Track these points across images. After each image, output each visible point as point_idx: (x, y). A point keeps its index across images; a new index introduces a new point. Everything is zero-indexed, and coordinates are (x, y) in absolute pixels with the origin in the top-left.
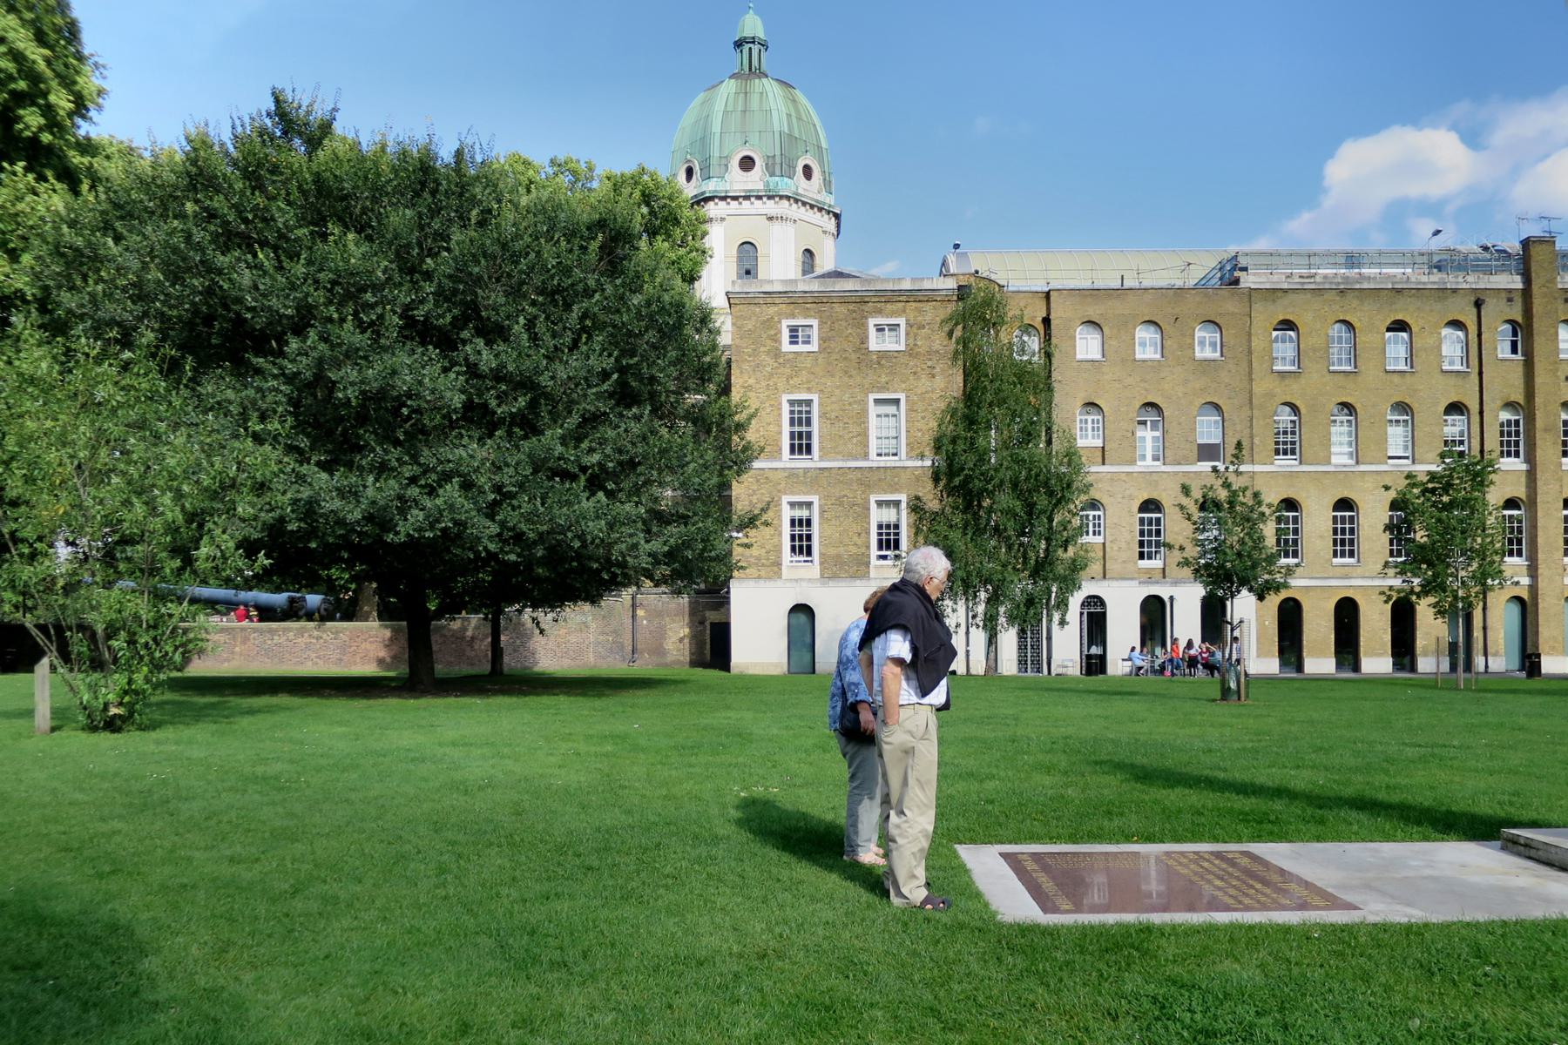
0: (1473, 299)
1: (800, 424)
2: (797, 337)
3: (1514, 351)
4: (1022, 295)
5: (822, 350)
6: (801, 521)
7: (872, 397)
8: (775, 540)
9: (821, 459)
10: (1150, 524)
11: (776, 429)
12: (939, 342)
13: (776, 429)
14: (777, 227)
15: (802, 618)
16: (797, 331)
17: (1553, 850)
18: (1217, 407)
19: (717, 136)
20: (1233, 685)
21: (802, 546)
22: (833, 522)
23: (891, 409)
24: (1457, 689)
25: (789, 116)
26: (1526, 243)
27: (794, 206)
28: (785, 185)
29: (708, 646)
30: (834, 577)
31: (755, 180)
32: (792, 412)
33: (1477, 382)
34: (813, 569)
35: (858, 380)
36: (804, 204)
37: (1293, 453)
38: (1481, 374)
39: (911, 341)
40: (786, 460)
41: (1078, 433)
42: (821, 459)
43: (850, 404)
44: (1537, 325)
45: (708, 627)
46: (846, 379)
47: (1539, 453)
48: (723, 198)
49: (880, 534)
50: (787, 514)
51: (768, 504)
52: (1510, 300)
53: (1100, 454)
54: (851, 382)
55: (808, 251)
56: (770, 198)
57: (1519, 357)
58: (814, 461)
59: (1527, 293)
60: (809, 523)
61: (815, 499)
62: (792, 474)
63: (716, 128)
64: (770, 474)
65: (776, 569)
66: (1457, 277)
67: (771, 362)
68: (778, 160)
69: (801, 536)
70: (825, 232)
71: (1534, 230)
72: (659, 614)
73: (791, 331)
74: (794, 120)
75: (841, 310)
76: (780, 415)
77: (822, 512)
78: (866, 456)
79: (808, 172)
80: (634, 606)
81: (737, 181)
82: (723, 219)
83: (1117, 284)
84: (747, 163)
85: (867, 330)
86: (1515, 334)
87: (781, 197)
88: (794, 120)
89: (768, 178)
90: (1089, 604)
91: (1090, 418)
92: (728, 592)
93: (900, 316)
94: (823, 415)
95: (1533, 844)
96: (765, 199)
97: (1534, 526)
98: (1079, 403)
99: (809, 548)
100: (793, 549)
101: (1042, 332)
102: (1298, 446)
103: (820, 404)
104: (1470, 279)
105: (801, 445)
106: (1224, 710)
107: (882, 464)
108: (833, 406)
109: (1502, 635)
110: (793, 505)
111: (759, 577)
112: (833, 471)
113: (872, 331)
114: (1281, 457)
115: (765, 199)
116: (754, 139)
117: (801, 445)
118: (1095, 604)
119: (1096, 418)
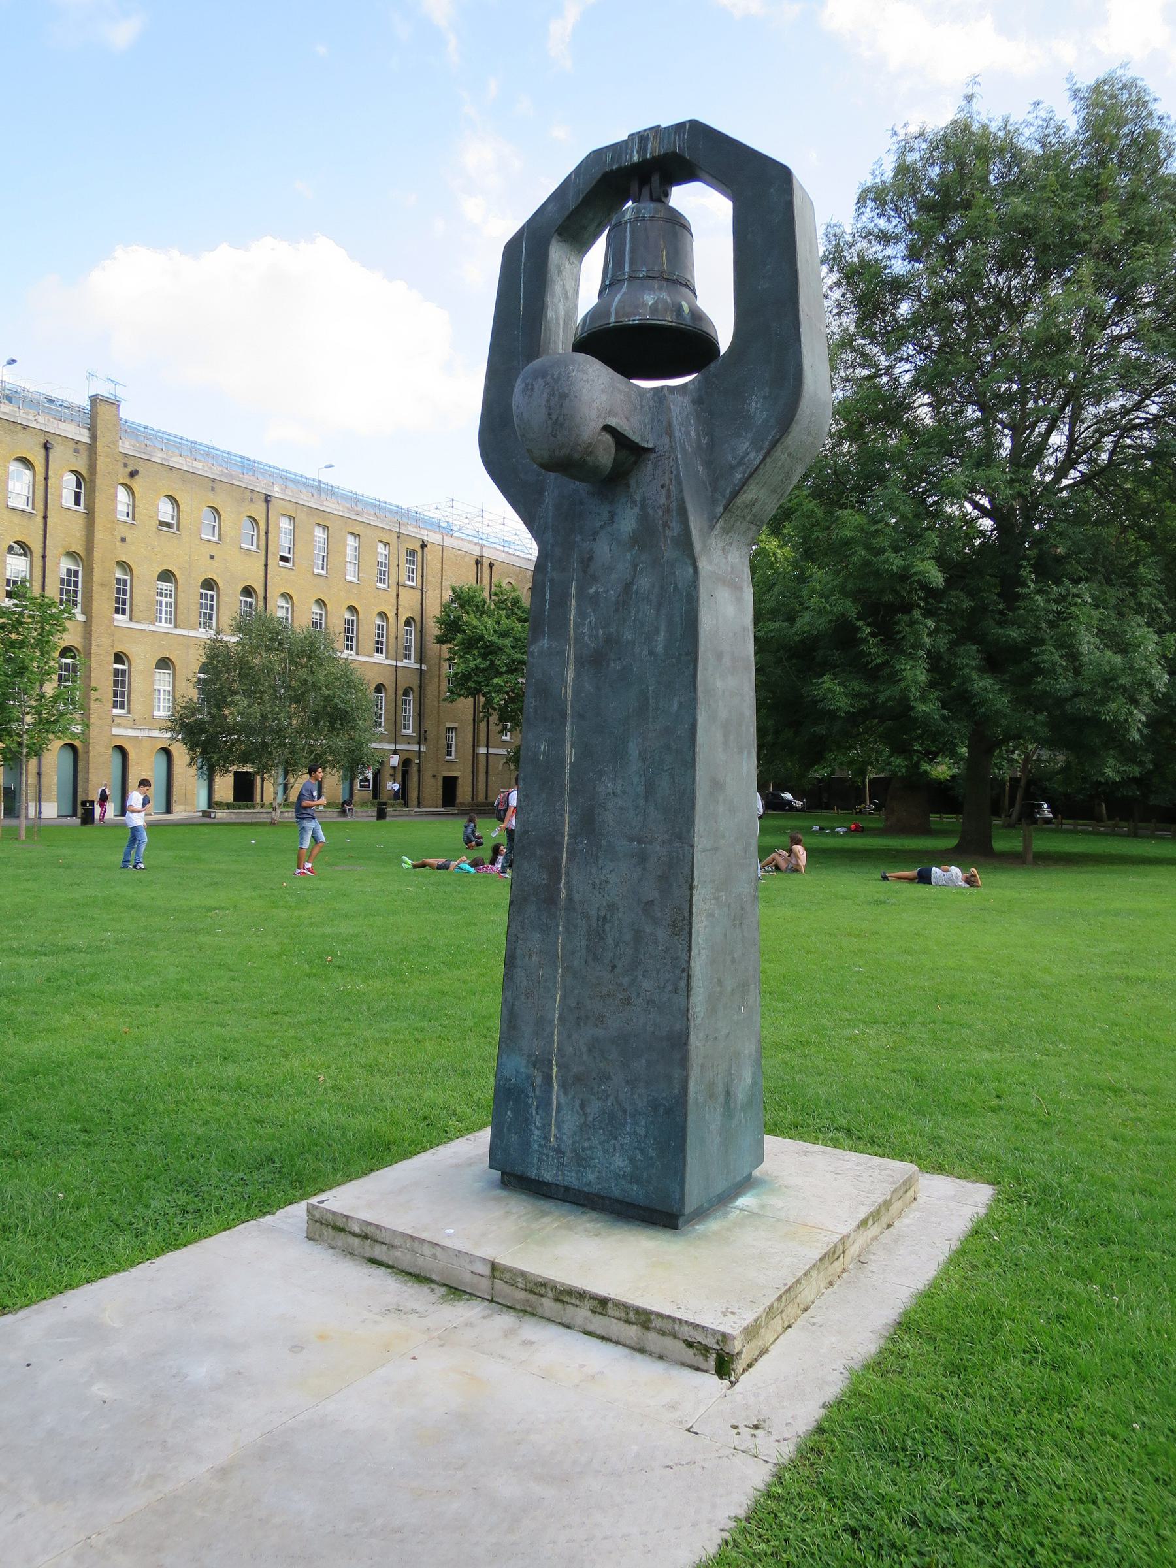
0: (42, 441)
3: (77, 502)
17: (427, 1250)
24: (17, 838)
26: (95, 400)
33: (41, 525)
38: (45, 518)
44: (99, 481)
47: (95, 606)
51: (870, 903)
52: (76, 451)
57: (81, 508)
59: (92, 447)
66: (27, 414)
71: (104, 391)
86: (79, 486)
95: (381, 1236)
97: (130, 672)
104: (40, 419)
109: (55, 781)
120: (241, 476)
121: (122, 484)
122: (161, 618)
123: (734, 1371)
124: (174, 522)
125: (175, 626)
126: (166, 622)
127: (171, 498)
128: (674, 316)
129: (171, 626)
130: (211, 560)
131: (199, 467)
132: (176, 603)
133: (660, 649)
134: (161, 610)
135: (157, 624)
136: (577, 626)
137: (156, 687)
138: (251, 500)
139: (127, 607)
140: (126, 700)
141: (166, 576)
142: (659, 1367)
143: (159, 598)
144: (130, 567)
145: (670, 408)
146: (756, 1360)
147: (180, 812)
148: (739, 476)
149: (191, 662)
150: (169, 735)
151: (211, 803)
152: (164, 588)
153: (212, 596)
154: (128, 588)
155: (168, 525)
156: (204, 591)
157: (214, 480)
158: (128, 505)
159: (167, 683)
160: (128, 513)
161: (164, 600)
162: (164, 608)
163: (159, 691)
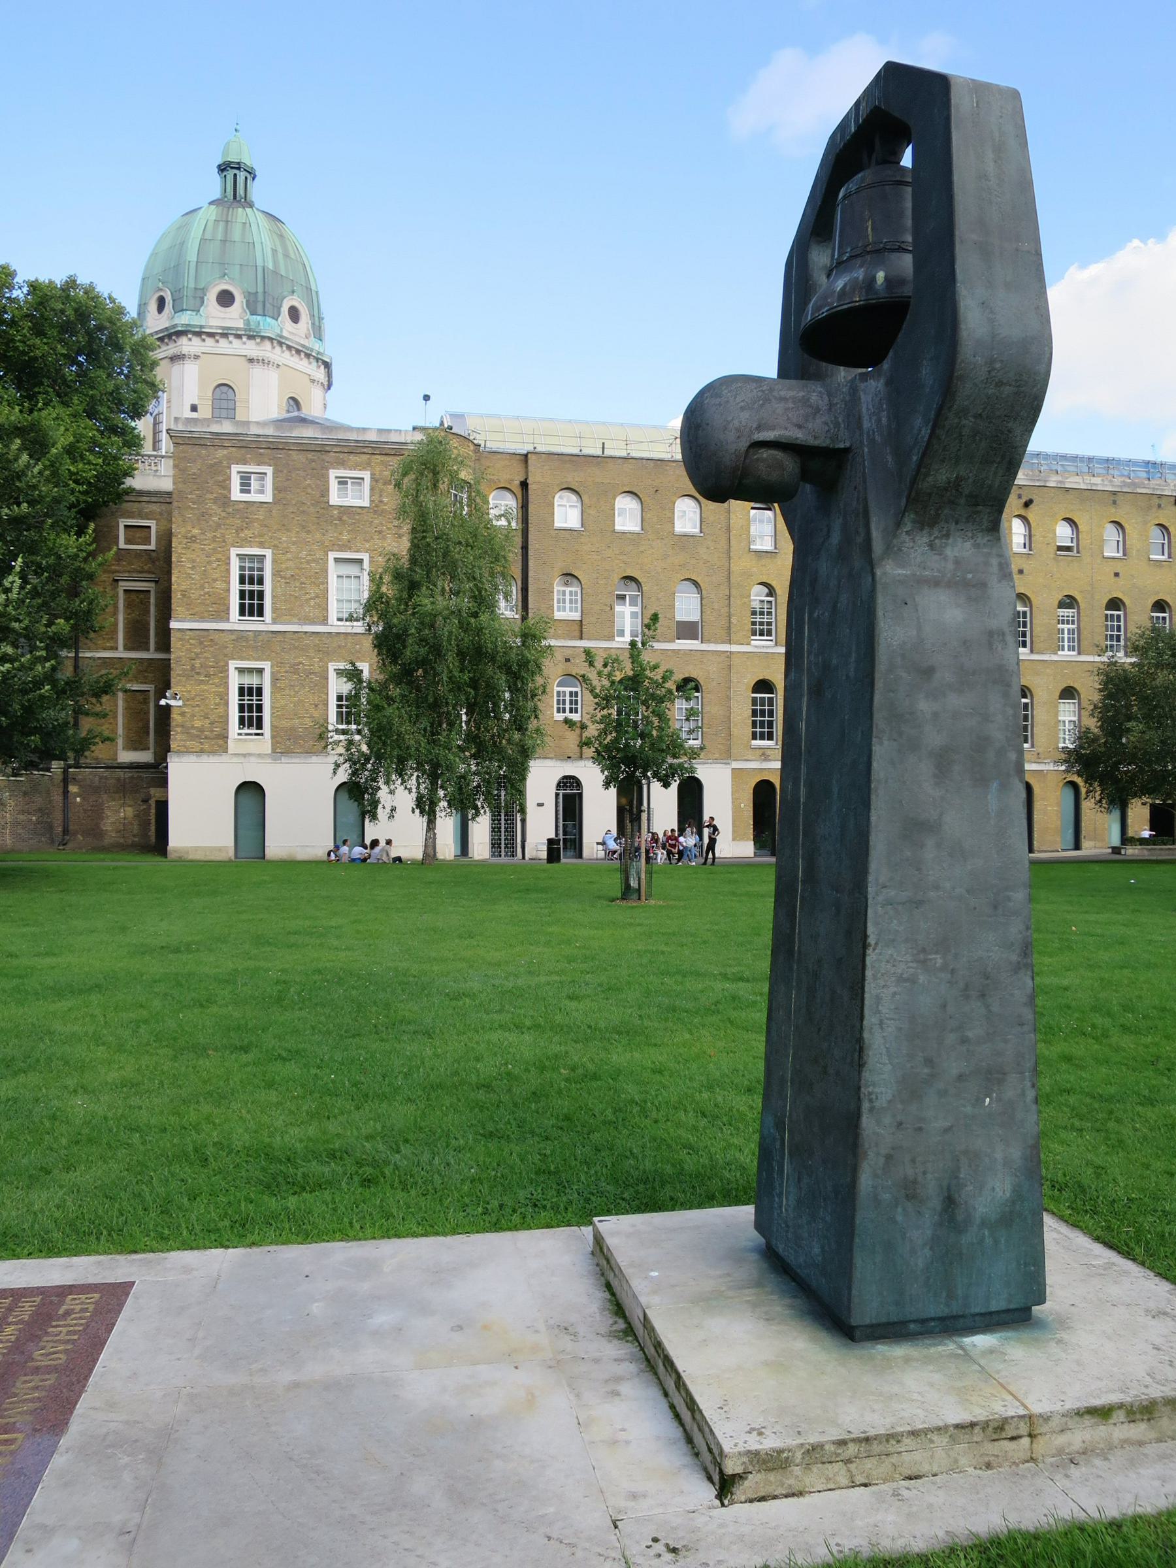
1: (251, 582)
2: (249, 485)
4: (499, 456)
5: (277, 501)
6: (250, 689)
7: (332, 556)
8: (221, 710)
9: (275, 621)
10: (763, 704)
11: (224, 586)
12: (391, 500)
13: (224, 586)
14: (257, 371)
15: (248, 799)
16: (249, 478)
18: (695, 583)
19: (193, 265)
20: (634, 883)
21: (251, 718)
22: (287, 692)
23: (352, 570)
25: (274, 251)
27: (278, 349)
28: (268, 326)
29: (153, 828)
30: (287, 752)
31: (234, 316)
32: (242, 568)
34: (264, 742)
35: (318, 536)
36: (289, 348)
37: (769, 633)
39: (376, 497)
40: (235, 620)
41: (556, 605)
42: (275, 621)
43: (308, 562)
45: (153, 806)
46: (304, 535)
48: (198, 334)
49: (339, 706)
50: (234, 681)
53: (577, 628)
54: (309, 538)
55: (292, 398)
56: (250, 337)
58: (266, 623)
60: (259, 691)
61: (266, 665)
62: (240, 636)
63: (192, 256)
64: (216, 637)
65: (221, 742)
67: (219, 511)
68: (260, 298)
69: (250, 706)
70: (313, 381)
72: (96, 790)
73: (242, 478)
74: (280, 256)
75: (299, 458)
76: (228, 571)
77: (275, 680)
78: (324, 621)
79: (294, 315)
80: (66, 781)
81: (213, 315)
82: (197, 357)
83: (599, 453)
84: (226, 299)
85: (328, 482)
87: (263, 338)
88: (280, 256)
89: (248, 316)
90: (565, 784)
91: (568, 590)
92: (166, 767)
93: (364, 469)
94: (275, 574)
96: (244, 339)
98: (557, 571)
99: (260, 719)
100: (242, 721)
101: (520, 496)
102: (773, 627)
103: (274, 561)
105: (252, 605)
106: (622, 912)
107: (342, 630)
108: (291, 564)
110: (241, 671)
111: (202, 751)
112: (288, 635)
113: (333, 485)
114: (758, 637)
115: (244, 339)
116: (235, 271)
117: (252, 605)
118: (572, 785)
119: (573, 589)
120: (1146, 482)
121: (1018, 516)
122: (1063, 646)
123: (732, 1494)
124: (1074, 544)
125: (1079, 653)
126: (1069, 650)
127: (1070, 521)
128: (864, 294)
129: (1075, 653)
130: (1117, 578)
131: (1098, 483)
132: (1079, 628)
133: (852, 674)
134: (1063, 638)
135: (1060, 653)
136: (808, 657)
137: (1060, 718)
138: (1159, 506)
139: (1028, 639)
140: (1029, 734)
141: (1069, 602)
142: (688, 1459)
143: (1060, 626)
144: (1029, 599)
145: (860, 398)
146: (775, 1497)
147: (1089, 848)
148: (915, 458)
149: (1091, 691)
150: (1063, 768)
151: (1126, 840)
152: (1066, 614)
153: (1119, 617)
154: (1028, 619)
155: (1068, 549)
156: (1109, 612)
157: (1114, 493)
158: (1025, 536)
159: (1072, 714)
160: (1025, 544)
161: (1066, 627)
162: (1066, 636)
163: (1064, 722)
